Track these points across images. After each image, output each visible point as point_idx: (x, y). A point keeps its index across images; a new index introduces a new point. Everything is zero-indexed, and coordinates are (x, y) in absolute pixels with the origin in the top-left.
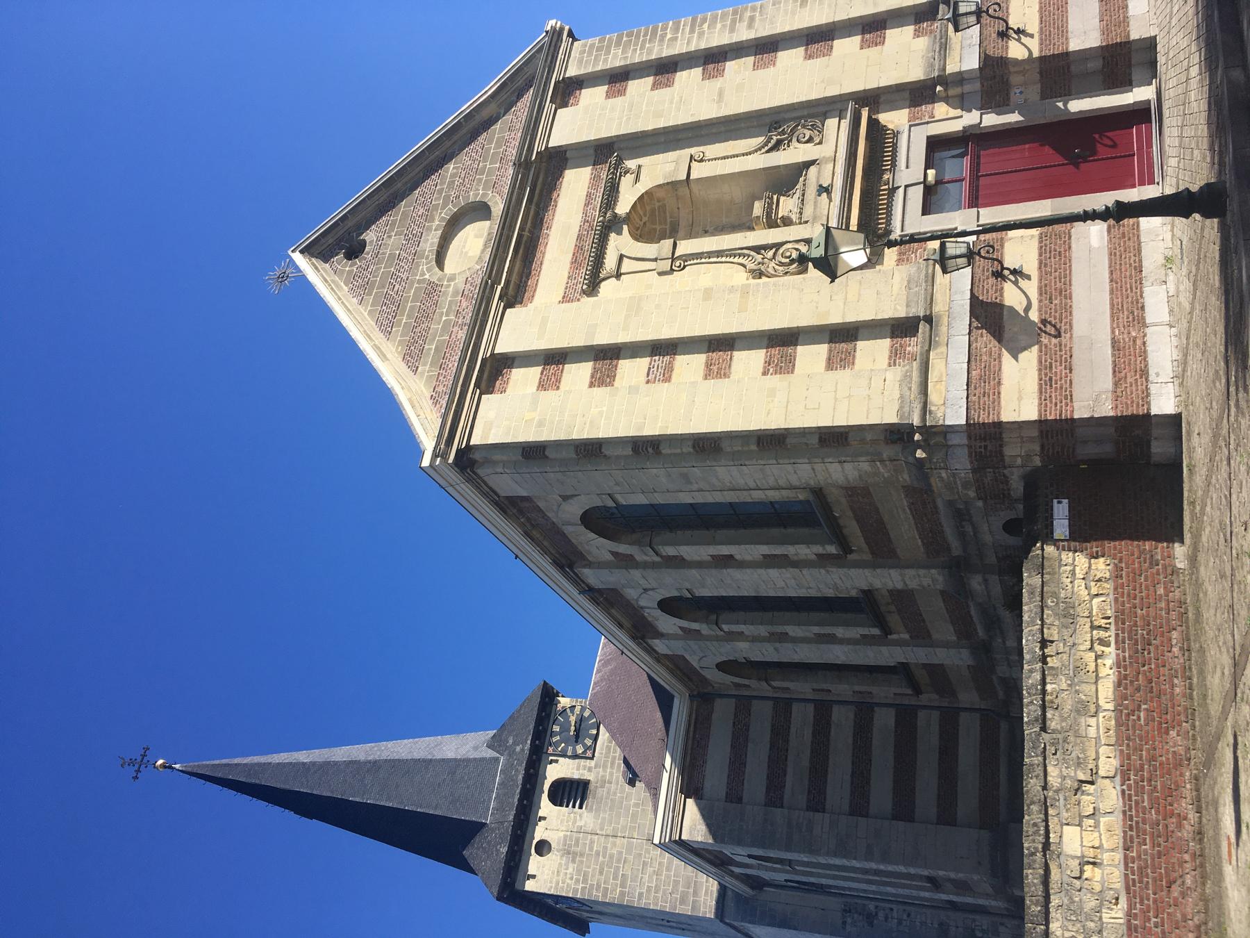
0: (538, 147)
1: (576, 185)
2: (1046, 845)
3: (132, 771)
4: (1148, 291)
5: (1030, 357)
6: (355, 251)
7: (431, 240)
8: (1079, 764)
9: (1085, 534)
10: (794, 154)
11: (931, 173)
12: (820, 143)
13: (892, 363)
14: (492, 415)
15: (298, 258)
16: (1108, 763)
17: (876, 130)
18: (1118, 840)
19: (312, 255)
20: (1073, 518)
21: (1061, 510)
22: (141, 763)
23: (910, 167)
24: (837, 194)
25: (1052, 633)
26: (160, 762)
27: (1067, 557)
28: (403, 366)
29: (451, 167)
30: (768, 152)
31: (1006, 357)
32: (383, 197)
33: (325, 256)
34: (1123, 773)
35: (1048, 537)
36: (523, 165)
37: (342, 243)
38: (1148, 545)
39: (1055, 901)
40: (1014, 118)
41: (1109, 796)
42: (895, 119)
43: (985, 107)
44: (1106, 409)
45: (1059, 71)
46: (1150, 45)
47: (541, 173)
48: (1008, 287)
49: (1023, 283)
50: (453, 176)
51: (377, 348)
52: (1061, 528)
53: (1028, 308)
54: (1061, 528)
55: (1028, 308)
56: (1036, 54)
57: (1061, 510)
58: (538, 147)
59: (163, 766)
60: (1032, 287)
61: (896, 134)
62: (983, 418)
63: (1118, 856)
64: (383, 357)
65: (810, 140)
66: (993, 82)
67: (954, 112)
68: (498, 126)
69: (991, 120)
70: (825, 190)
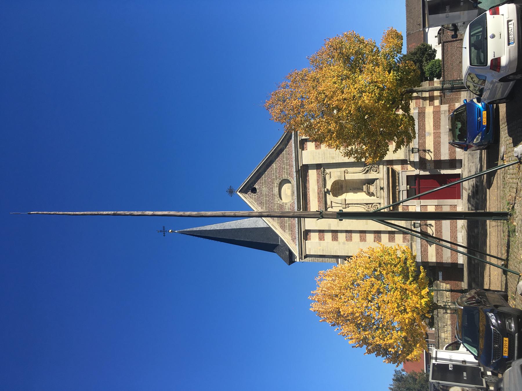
0: (300, 165)
1: (312, 174)
2: (439, 336)
3: (162, 233)
4: (458, 234)
5: (434, 246)
6: (254, 191)
7: (276, 190)
8: (444, 323)
9: (445, 279)
10: (372, 175)
11: (408, 186)
12: (379, 173)
13: (404, 242)
14: (310, 247)
15: (238, 193)
16: (449, 322)
17: (393, 171)
18: (450, 335)
19: (242, 192)
20: (443, 275)
21: (440, 274)
22: (164, 231)
23: (403, 186)
24: (386, 190)
25: (439, 299)
26: (170, 231)
27: (442, 284)
28: (280, 229)
29: (274, 165)
30: (366, 173)
31: (429, 246)
32: (257, 175)
33: (246, 192)
34: (452, 324)
35: (438, 280)
36: (297, 172)
37: (250, 188)
38: (457, 282)
39: (440, 345)
40: (427, 173)
41: (449, 328)
42: (398, 168)
43: (420, 169)
44: (449, 261)
45: (439, 164)
46: (461, 161)
47: (303, 172)
48: (428, 228)
49: (432, 227)
50: (276, 169)
51: (273, 225)
52: (440, 278)
53: (433, 234)
54: (440, 278)
55: (433, 234)
56: (433, 159)
57: (440, 274)
58: (300, 165)
59: (172, 231)
60: (433, 229)
61: (398, 174)
62: (425, 261)
63: (451, 338)
64: (276, 229)
65: (376, 171)
66: (422, 164)
67: (413, 169)
68: (284, 152)
69: (422, 173)
70: (382, 189)
